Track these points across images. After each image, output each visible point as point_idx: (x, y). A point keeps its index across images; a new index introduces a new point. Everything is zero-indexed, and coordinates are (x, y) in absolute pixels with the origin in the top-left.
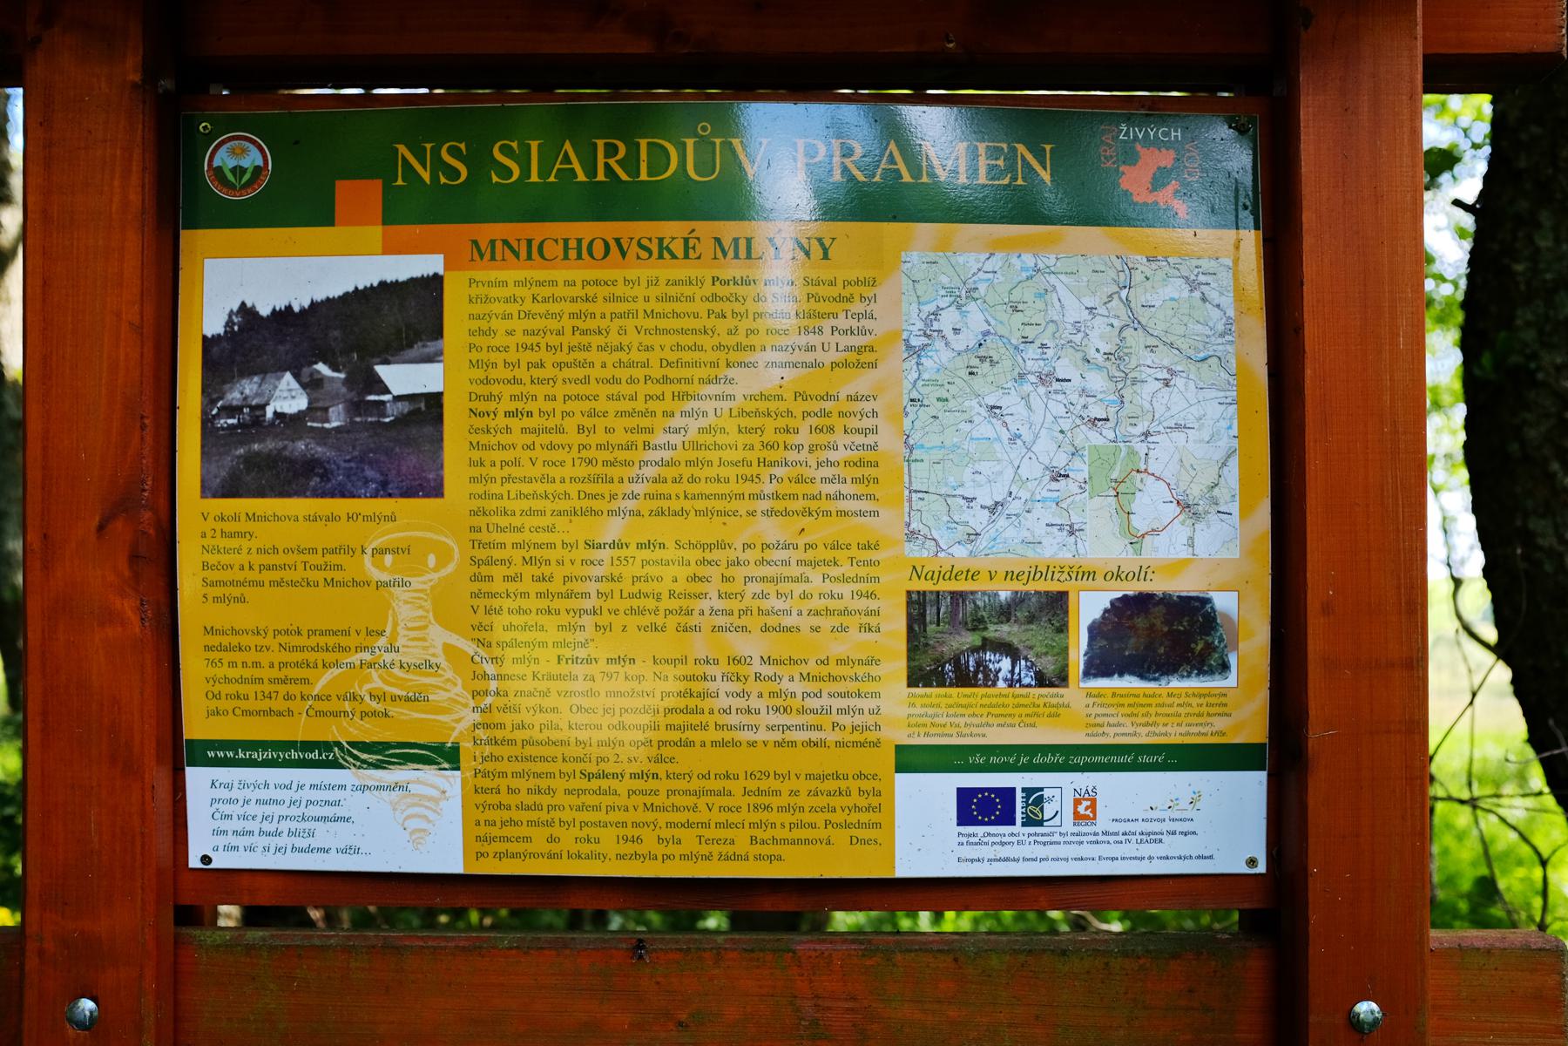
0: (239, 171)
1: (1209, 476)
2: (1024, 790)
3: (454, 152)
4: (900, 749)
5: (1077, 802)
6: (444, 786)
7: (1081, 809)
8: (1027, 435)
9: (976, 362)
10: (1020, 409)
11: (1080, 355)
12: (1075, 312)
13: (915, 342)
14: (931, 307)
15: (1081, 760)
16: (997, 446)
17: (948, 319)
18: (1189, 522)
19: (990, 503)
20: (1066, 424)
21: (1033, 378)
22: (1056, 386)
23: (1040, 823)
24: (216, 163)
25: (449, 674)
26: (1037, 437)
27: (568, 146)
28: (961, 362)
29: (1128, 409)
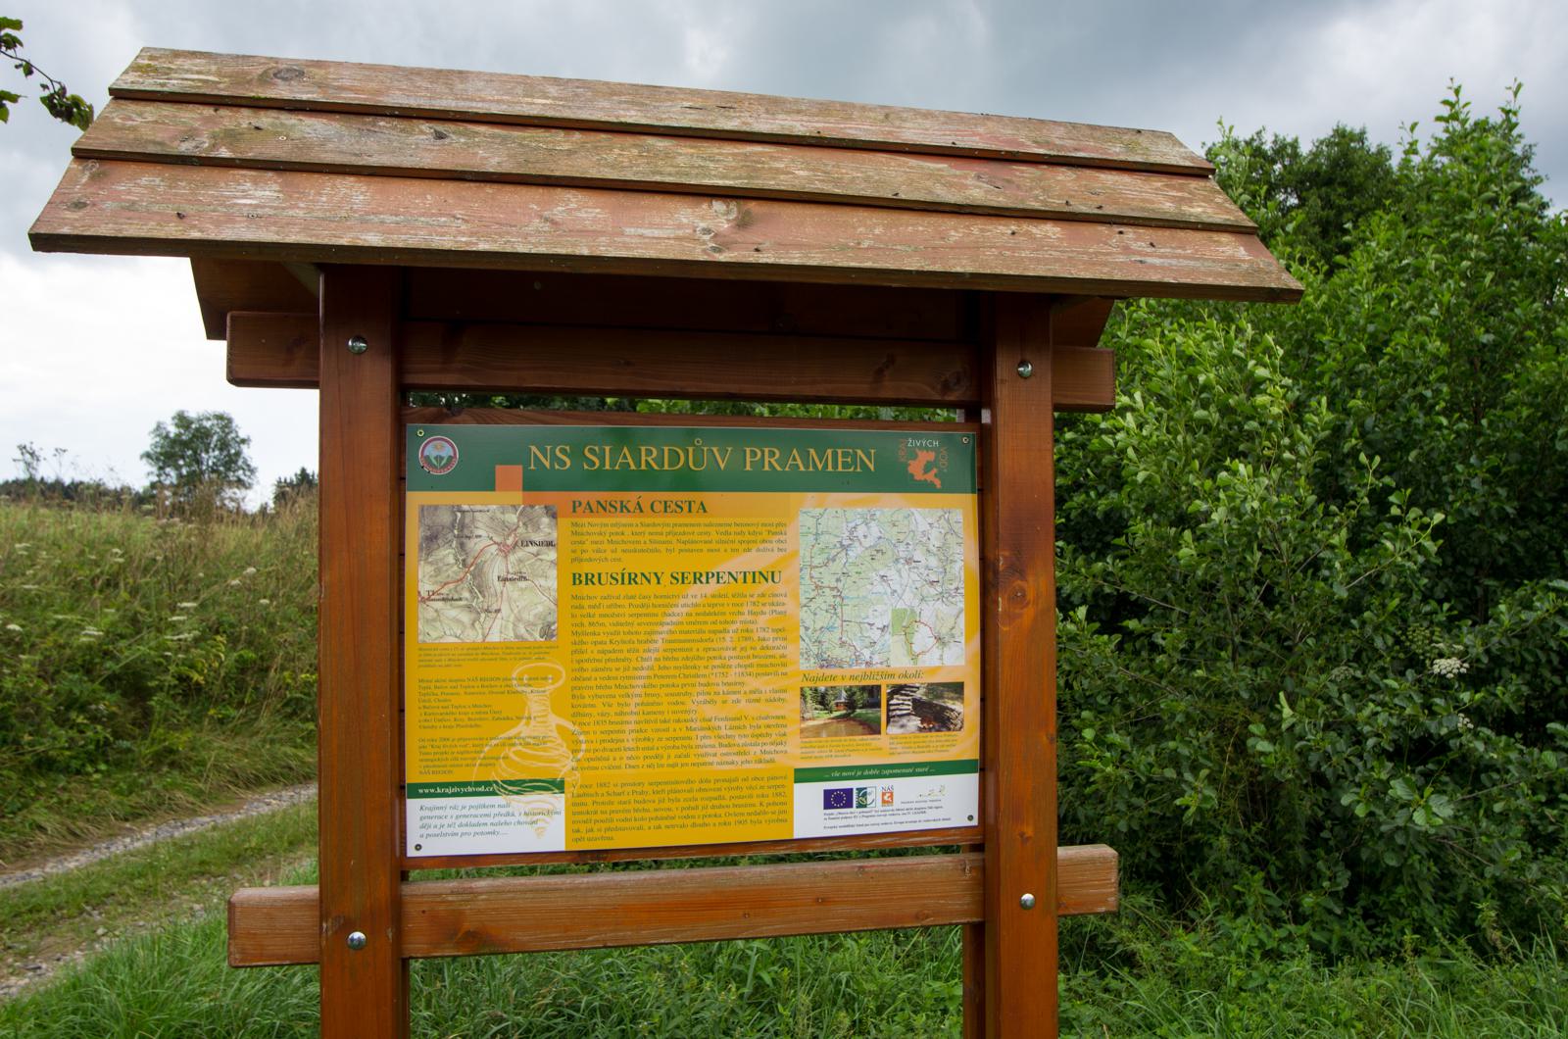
0: (439, 458)
3: (563, 451)
4: (797, 771)
6: (557, 801)
10: (896, 577)
12: (923, 526)
13: (845, 543)
17: (861, 531)
20: (918, 585)
24: (426, 453)
25: (560, 741)
27: (625, 450)
28: (867, 553)
29: (948, 576)
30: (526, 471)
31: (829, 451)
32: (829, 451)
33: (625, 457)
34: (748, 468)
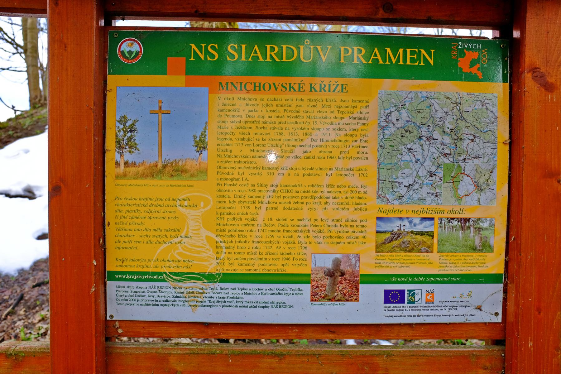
0: (130, 53)
2: (408, 290)
5: (427, 295)
8: (422, 160)
10: (420, 150)
11: (442, 129)
14: (388, 111)
16: (411, 164)
17: (393, 117)
19: (407, 185)
21: (424, 138)
22: (433, 141)
23: (414, 303)
25: (208, 247)
26: (425, 160)
27: (256, 47)
28: (398, 132)
31: (401, 50)
32: (401, 50)
33: (256, 52)
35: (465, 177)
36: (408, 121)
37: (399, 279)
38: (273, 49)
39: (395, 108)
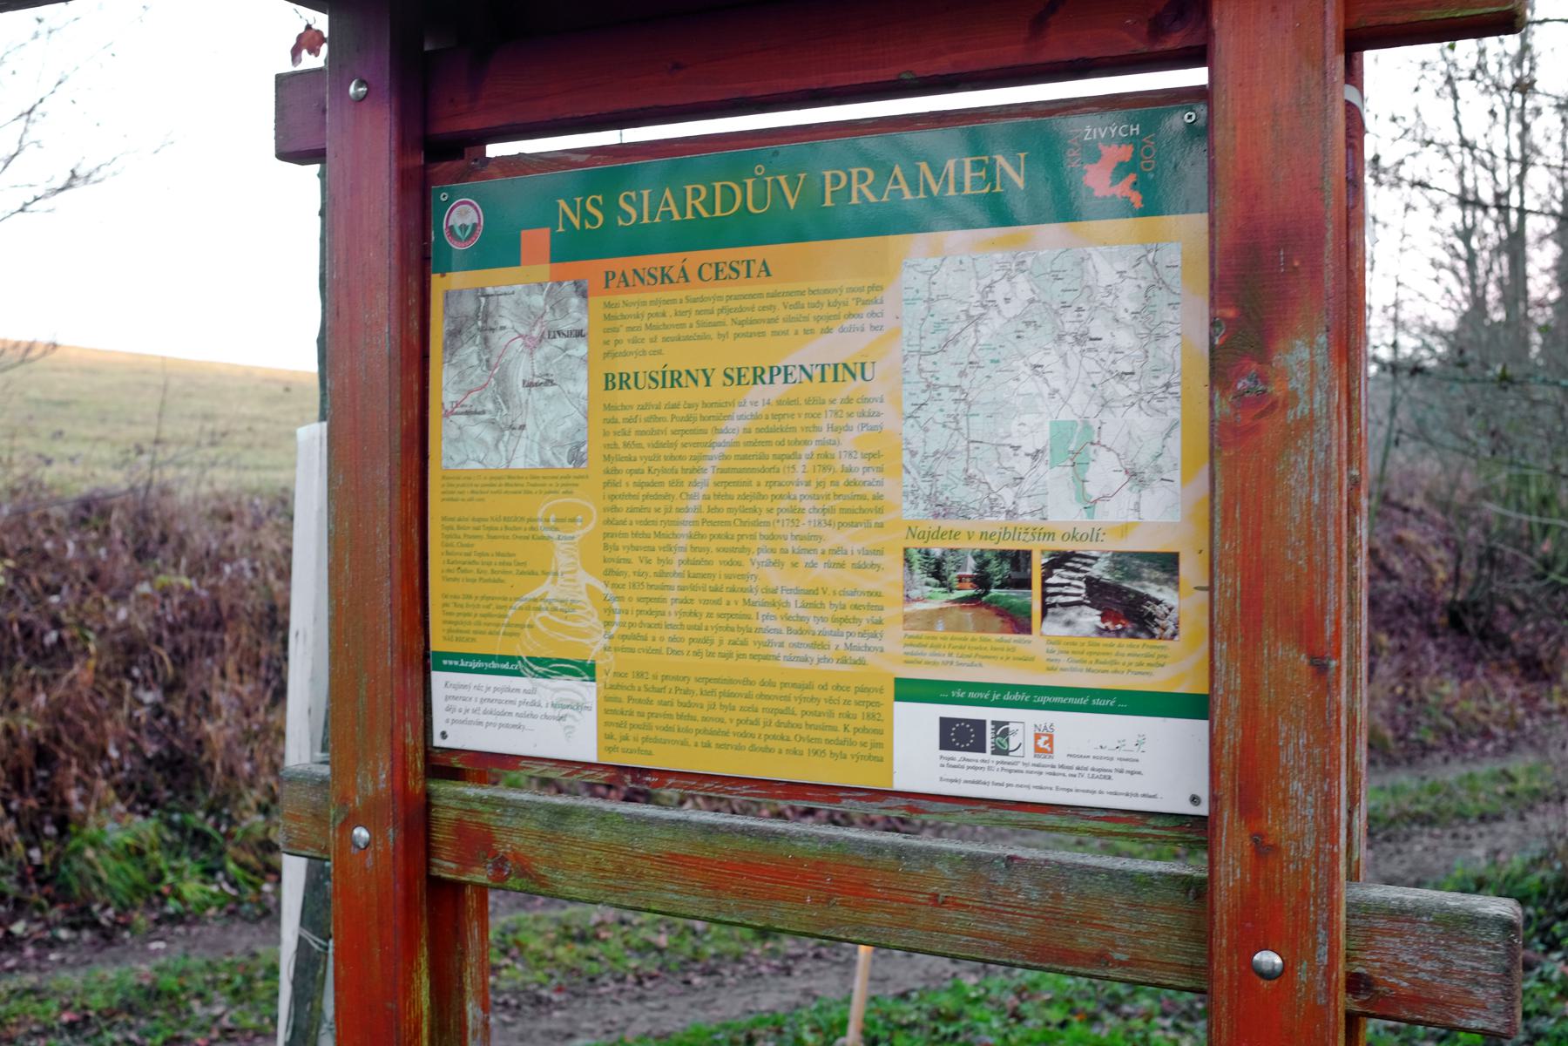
0: (464, 227)
1: (1155, 446)
2: (993, 723)
3: (595, 203)
5: (1037, 737)
7: (1041, 743)
8: (1064, 392)
9: (1022, 327)
11: (1110, 315)
14: (987, 281)
15: (1044, 700)
16: (1039, 401)
18: (1136, 489)
19: (1032, 451)
20: (1097, 379)
21: (1069, 339)
22: (1090, 344)
23: (1006, 753)
25: (590, 608)
26: (1072, 391)
27: (667, 193)
30: (555, 236)
34: (828, 203)
35: (1102, 451)
36: (1032, 301)
37: (972, 695)
38: (697, 193)
39: (1001, 273)
